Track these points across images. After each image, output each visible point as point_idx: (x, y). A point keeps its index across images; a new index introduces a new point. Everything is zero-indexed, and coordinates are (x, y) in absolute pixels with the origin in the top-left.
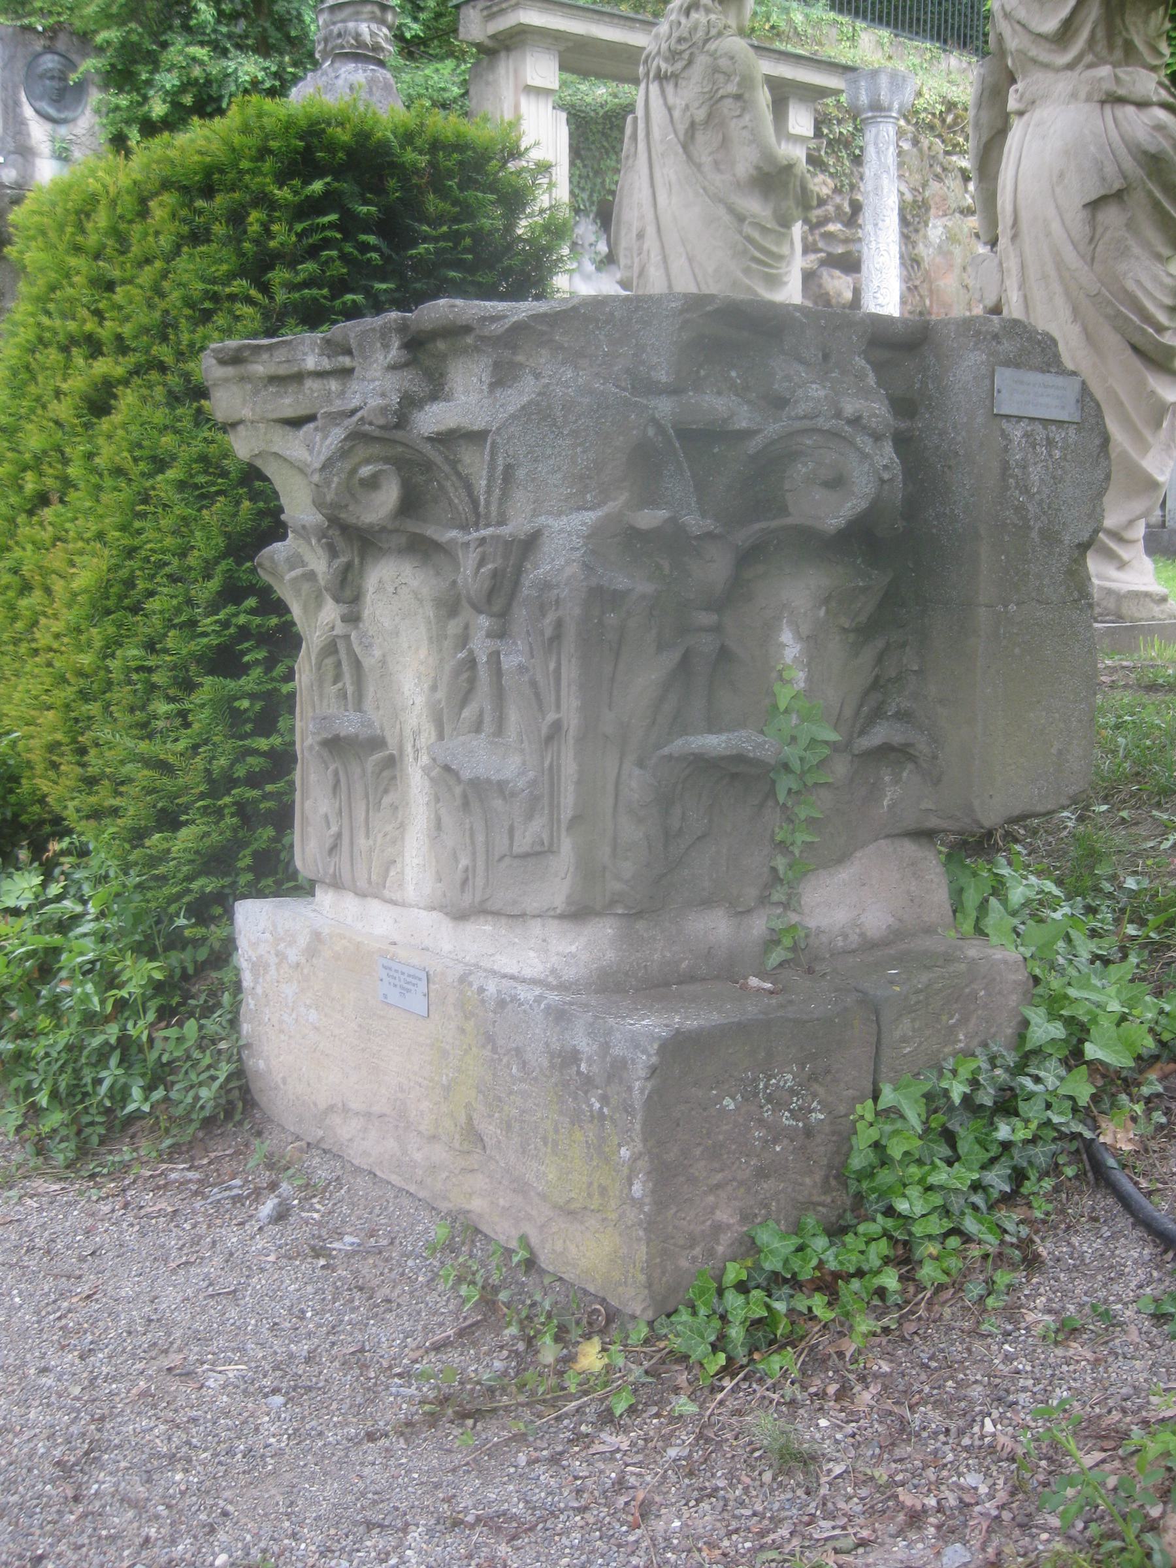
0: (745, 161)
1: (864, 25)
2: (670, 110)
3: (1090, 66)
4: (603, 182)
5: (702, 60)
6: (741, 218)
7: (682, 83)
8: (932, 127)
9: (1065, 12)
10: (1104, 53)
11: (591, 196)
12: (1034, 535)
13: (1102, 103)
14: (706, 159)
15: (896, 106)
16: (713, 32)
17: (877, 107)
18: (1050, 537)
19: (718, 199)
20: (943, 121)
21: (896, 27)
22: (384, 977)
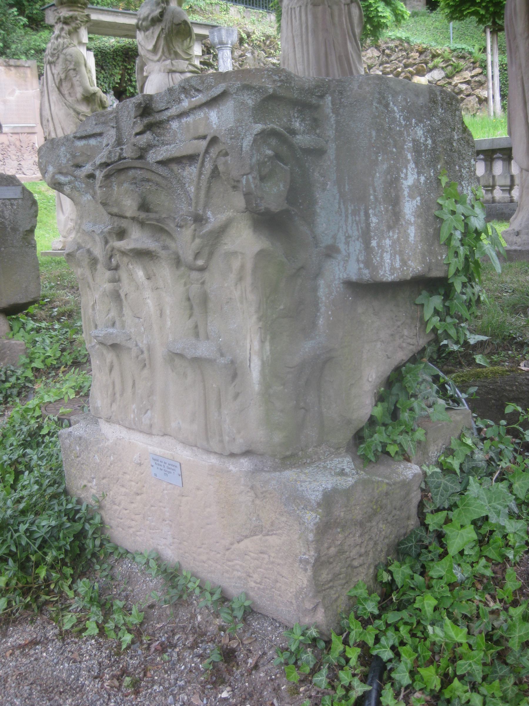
0: (79, 93)
1: (232, 4)
2: (53, 75)
3: (164, 60)
4: (114, 80)
5: (62, 56)
6: (78, 113)
7: (57, 65)
8: (259, 47)
9: (154, 43)
10: (168, 56)
11: (109, 85)
12: (9, 229)
13: (168, 73)
14: (66, 92)
15: (230, 42)
16: (65, 46)
17: (221, 43)
18: (14, 230)
19: (69, 107)
20: (265, 44)
21: (246, 4)
22: (153, 464)
